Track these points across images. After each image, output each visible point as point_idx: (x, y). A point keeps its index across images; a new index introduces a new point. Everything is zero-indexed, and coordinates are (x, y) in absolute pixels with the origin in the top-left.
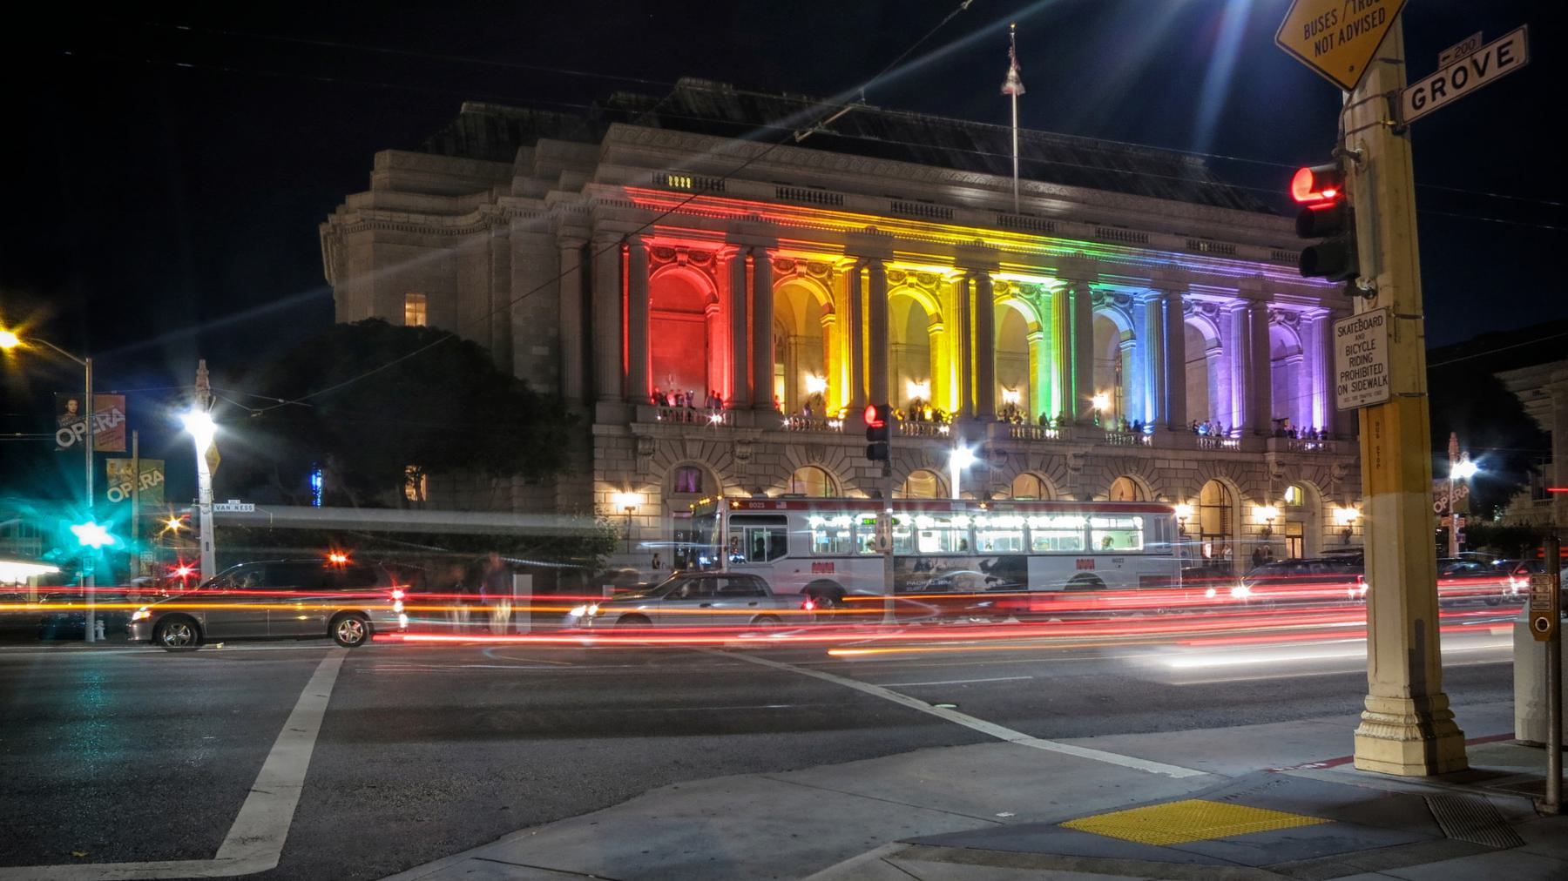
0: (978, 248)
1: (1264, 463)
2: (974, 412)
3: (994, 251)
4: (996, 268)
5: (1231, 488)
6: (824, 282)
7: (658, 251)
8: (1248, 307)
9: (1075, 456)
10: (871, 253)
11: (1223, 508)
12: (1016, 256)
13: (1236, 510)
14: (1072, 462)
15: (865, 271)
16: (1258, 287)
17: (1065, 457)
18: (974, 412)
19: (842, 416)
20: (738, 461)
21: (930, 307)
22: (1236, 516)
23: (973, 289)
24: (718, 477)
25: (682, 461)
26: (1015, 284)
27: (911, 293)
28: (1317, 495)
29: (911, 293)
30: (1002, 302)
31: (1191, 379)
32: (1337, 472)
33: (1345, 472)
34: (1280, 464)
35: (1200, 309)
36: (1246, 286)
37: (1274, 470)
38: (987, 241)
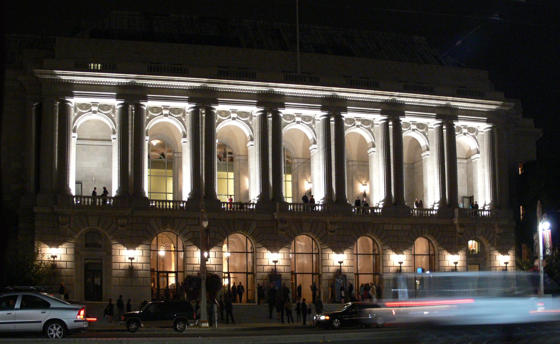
0: (271, 95)
1: (453, 225)
2: (393, 201)
3: (281, 96)
4: (283, 106)
5: (433, 242)
6: (369, 130)
7: (153, 109)
8: (442, 124)
9: (331, 223)
10: (204, 100)
11: (429, 255)
12: (296, 99)
13: (436, 257)
14: (329, 227)
15: (332, 119)
16: (448, 113)
17: (327, 223)
18: (271, 197)
19: (381, 206)
20: (119, 228)
21: (368, 138)
22: (437, 261)
23: (391, 127)
24: (110, 237)
25: (87, 228)
26: (414, 123)
27: (357, 130)
28: (487, 245)
29: (357, 130)
30: (407, 134)
31: (461, 172)
32: (497, 230)
33: (502, 231)
34: (462, 226)
35: (359, 123)
36: (441, 112)
37: (458, 230)
38: (276, 90)
